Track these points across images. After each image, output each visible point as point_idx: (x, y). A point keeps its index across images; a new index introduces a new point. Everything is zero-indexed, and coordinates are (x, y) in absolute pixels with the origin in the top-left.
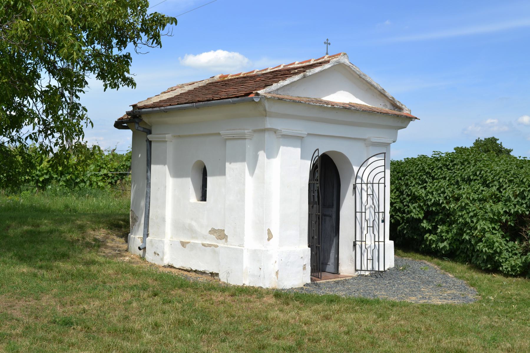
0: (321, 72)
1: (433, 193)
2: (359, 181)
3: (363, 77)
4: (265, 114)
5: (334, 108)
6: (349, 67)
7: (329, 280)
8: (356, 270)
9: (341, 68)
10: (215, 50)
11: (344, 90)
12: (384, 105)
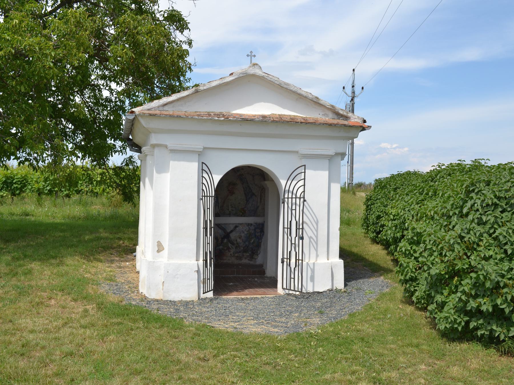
3: (285, 86)
6: (263, 77)
7: (258, 296)
11: (265, 102)
12: (324, 115)
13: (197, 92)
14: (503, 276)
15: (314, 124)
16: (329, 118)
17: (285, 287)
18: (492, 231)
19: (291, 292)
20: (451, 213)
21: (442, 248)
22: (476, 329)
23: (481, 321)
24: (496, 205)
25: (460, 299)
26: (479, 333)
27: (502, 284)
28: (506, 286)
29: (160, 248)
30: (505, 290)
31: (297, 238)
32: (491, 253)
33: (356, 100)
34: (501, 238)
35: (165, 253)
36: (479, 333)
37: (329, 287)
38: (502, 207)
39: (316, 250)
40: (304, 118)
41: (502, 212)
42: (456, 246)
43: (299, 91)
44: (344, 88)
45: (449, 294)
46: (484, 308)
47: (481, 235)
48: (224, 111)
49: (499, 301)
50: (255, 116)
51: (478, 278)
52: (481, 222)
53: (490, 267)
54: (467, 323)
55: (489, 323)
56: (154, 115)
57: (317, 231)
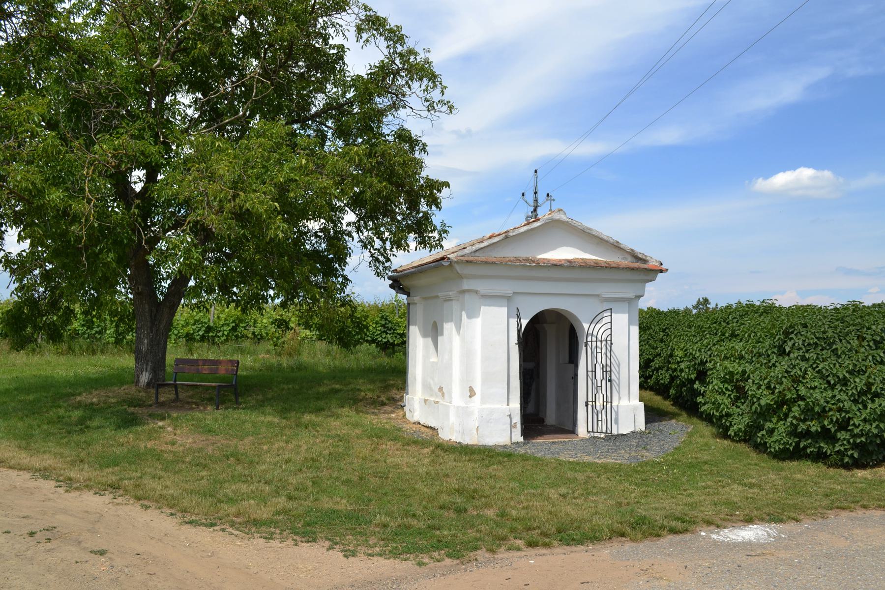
0: (528, 231)
1: (684, 350)
2: (589, 339)
4: (461, 277)
5: (556, 266)
8: (588, 432)
9: (554, 224)
10: (795, 168)
13: (507, 237)
14: (828, 402)
15: (617, 268)
16: (627, 262)
17: (590, 429)
18: (814, 366)
19: (596, 435)
20: (769, 353)
21: (769, 382)
22: (805, 447)
23: (810, 441)
24: (816, 344)
25: (792, 423)
26: (809, 451)
27: (827, 409)
28: (831, 409)
29: (472, 393)
30: (831, 413)
31: (604, 382)
32: (816, 384)
33: (539, 210)
34: (824, 371)
35: (477, 398)
36: (809, 451)
37: (632, 429)
38: (821, 345)
39: (619, 393)
40: (605, 262)
41: (822, 350)
42: (784, 379)
43: (601, 236)
44: (523, 195)
45: (778, 422)
46: (813, 429)
47: (806, 370)
48: (530, 256)
49: (826, 423)
50: (560, 261)
51: (807, 404)
52: (804, 359)
53: (817, 394)
54: (798, 444)
55: (817, 442)
56: (471, 262)
57: (619, 373)
